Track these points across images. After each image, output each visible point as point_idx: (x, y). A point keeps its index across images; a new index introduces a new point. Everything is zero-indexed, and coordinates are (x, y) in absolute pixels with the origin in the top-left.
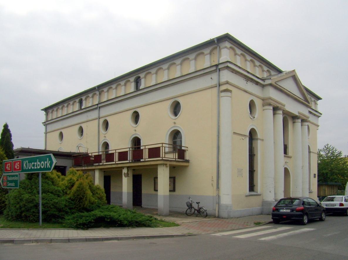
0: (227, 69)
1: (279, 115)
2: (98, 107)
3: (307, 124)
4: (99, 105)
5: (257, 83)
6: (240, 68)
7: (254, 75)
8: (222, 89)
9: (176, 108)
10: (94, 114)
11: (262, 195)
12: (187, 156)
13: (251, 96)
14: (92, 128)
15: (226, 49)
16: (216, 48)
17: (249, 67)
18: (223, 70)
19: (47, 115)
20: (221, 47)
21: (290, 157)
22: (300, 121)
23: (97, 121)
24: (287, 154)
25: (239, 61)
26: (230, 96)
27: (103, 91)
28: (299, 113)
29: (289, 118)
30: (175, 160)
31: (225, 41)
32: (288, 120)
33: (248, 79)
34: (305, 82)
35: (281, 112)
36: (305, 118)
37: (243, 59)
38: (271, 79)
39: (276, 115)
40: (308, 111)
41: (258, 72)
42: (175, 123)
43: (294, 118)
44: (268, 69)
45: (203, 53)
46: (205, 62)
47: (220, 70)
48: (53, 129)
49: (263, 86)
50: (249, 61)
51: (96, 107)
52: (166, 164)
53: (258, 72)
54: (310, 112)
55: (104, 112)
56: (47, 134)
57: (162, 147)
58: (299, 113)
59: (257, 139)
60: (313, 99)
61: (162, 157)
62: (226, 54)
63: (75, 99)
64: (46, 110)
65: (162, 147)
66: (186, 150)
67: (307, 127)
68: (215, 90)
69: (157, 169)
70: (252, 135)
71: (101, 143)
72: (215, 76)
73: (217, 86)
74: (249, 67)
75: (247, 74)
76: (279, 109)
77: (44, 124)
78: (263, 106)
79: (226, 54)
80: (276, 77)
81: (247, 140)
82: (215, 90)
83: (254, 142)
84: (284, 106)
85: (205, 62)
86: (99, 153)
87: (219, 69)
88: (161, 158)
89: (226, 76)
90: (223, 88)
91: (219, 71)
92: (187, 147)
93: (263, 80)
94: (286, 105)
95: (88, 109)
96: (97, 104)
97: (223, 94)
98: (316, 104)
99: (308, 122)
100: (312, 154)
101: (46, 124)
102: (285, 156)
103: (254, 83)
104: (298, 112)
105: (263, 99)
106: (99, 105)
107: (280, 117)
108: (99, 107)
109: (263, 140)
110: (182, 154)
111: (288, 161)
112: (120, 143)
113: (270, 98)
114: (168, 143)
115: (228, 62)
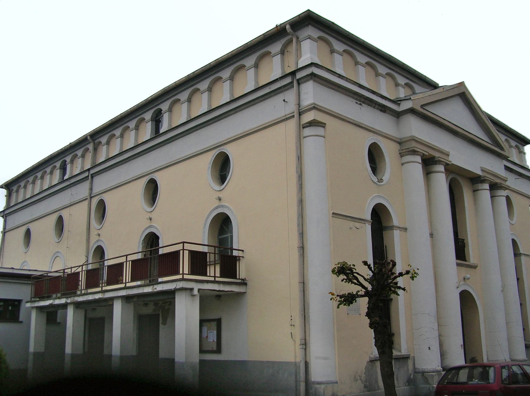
0: (312, 79)
1: (434, 174)
2: (89, 175)
3: (505, 193)
4: (92, 172)
5: (383, 109)
6: (340, 76)
7: (374, 92)
8: (309, 122)
9: (222, 167)
10: (82, 190)
11: (410, 362)
12: (242, 271)
13: (371, 134)
14: (77, 217)
15: (309, 40)
16: (290, 41)
17: (363, 77)
18: (305, 82)
19: (9, 196)
20: (301, 37)
21: (474, 267)
22: (487, 186)
23: (86, 203)
24: (467, 259)
25: (340, 64)
26: (323, 134)
27: (100, 142)
28: (483, 170)
29: (461, 181)
30: (213, 279)
31: (307, 25)
32: (461, 187)
33: (362, 100)
34: (488, 105)
35: (441, 168)
36: (498, 181)
37: (326, 49)
38: (410, 99)
39: (433, 175)
40: (503, 167)
41: (385, 88)
42: (220, 199)
43: (475, 180)
44: (407, 81)
45: (268, 53)
46: (273, 69)
47: (300, 81)
48: (17, 223)
49: (398, 115)
50: (402, 86)
51: (86, 174)
52: (192, 289)
53: (385, 88)
54: (507, 168)
55: (101, 183)
56: (7, 234)
57: (183, 250)
58: (483, 170)
59: (392, 228)
60: (513, 143)
61: (183, 274)
62: (309, 51)
63: (53, 163)
64: (9, 186)
65: (183, 250)
66: (239, 257)
67: (504, 199)
68: (292, 124)
69: (172, 304)
70: (379, 218)
71: (92, 248)
72: (290, 95)
73: (293, 116)
74: (363, 77)
75: (360, 89)
76: (436, 161)
77: (2, 214)
78: (402, 155)
79: (309, 51)
80: (421, 95)
81: (368, 228)
82: (292, 124)
83: (386, 234)
84: (448, 155)
85: (273, 69)
86: (215, 279)
87: (298, 80)
88: (180, 277)
89: (311, 93)
90: (308, 117)
91: (299, 84)
92: (243, 251)
93: (397, 102)
94: (452, 153)
95: (73, 181)
96: (89, 170)
97: (307, 131)
98: (522, 153)
99: (507, 189)
100: (523, 258)
101: (5, 214)
102: (458, 265)
103: (377, 109)
104: (481, 167)
105: (399, 141)
106: (92, 172)
107: (441, 180)
108: (92, 175)
109: (405, 229)
110: (229, 265)
111: (468, 276)
112: (123, 245)
113: (414, 139)
114: (207, 244)
115: (312, 64)
